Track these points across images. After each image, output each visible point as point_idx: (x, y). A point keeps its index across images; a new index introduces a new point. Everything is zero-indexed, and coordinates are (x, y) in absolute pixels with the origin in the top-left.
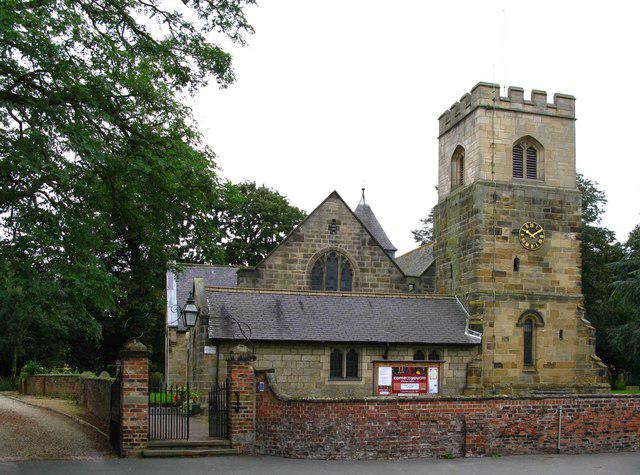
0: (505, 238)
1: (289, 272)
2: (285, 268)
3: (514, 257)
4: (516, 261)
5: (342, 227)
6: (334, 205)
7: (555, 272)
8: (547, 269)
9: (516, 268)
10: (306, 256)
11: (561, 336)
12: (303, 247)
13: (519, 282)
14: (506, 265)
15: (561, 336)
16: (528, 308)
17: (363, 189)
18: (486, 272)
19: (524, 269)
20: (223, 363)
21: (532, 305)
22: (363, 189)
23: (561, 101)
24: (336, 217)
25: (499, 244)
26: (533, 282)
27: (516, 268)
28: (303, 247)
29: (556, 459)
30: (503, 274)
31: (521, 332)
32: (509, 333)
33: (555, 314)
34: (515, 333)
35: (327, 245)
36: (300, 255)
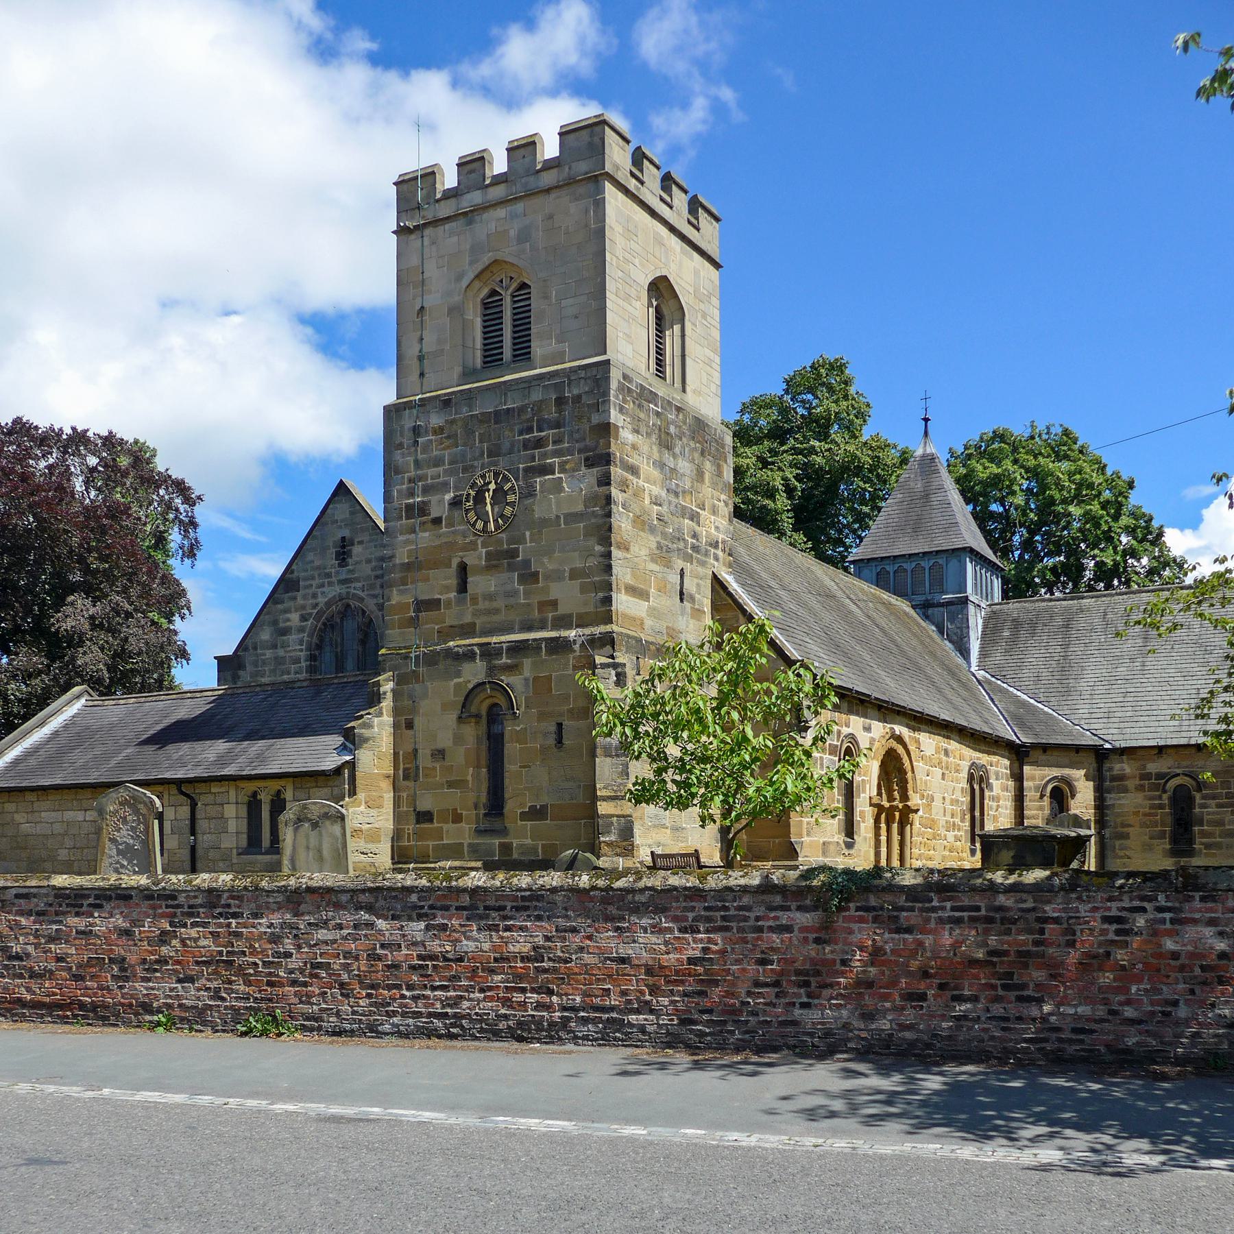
0: (437, 521)
1: (281, 653)
2: (275, 647)
3: (455, 562)
4: (463, 569)
5: (357, 550)
6: (341, 511)
7: (548, 577)
8: (529, 577)
9: (463, 588)
10: (304, 618)
11: (559, 741)
12: (300, 601)
13: (468, 619)
14: (440, 584)
15: (559, 741)
16: (481, 677)
17: (926, 420)
18: (403, 607)
19: (480, 584)
20: (744, 822)
21: (491, 670)
22: (926, 420)
23: (571, 137)
24: (346, 533)
25: (425, 537)
26: (497, 611)
27: (463, 588)
28: (300, 601)
29: (458, 1043)
30: (433, 604)
31: (472, 733)
32: (445, 740)
33: (541, 685)
34: (458, 739)
35: (334, 591)
36: (295, 617)
